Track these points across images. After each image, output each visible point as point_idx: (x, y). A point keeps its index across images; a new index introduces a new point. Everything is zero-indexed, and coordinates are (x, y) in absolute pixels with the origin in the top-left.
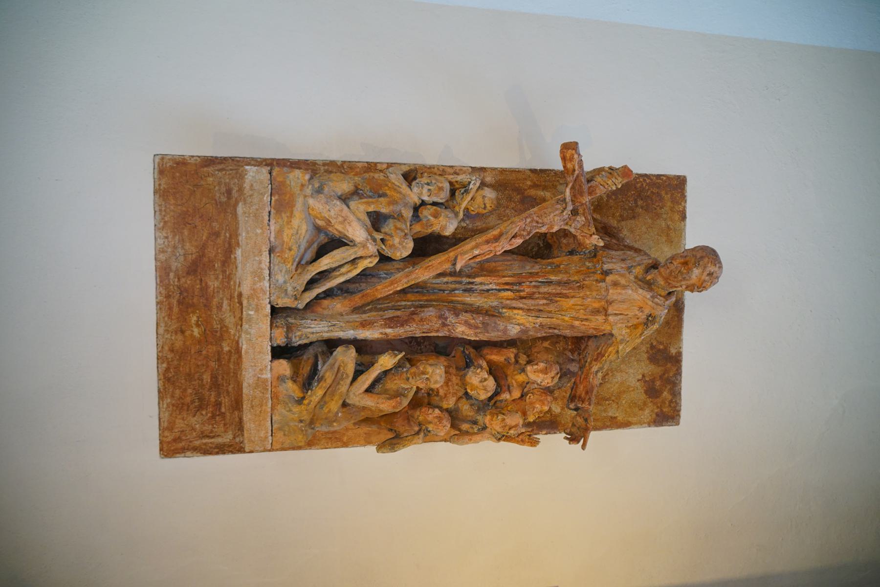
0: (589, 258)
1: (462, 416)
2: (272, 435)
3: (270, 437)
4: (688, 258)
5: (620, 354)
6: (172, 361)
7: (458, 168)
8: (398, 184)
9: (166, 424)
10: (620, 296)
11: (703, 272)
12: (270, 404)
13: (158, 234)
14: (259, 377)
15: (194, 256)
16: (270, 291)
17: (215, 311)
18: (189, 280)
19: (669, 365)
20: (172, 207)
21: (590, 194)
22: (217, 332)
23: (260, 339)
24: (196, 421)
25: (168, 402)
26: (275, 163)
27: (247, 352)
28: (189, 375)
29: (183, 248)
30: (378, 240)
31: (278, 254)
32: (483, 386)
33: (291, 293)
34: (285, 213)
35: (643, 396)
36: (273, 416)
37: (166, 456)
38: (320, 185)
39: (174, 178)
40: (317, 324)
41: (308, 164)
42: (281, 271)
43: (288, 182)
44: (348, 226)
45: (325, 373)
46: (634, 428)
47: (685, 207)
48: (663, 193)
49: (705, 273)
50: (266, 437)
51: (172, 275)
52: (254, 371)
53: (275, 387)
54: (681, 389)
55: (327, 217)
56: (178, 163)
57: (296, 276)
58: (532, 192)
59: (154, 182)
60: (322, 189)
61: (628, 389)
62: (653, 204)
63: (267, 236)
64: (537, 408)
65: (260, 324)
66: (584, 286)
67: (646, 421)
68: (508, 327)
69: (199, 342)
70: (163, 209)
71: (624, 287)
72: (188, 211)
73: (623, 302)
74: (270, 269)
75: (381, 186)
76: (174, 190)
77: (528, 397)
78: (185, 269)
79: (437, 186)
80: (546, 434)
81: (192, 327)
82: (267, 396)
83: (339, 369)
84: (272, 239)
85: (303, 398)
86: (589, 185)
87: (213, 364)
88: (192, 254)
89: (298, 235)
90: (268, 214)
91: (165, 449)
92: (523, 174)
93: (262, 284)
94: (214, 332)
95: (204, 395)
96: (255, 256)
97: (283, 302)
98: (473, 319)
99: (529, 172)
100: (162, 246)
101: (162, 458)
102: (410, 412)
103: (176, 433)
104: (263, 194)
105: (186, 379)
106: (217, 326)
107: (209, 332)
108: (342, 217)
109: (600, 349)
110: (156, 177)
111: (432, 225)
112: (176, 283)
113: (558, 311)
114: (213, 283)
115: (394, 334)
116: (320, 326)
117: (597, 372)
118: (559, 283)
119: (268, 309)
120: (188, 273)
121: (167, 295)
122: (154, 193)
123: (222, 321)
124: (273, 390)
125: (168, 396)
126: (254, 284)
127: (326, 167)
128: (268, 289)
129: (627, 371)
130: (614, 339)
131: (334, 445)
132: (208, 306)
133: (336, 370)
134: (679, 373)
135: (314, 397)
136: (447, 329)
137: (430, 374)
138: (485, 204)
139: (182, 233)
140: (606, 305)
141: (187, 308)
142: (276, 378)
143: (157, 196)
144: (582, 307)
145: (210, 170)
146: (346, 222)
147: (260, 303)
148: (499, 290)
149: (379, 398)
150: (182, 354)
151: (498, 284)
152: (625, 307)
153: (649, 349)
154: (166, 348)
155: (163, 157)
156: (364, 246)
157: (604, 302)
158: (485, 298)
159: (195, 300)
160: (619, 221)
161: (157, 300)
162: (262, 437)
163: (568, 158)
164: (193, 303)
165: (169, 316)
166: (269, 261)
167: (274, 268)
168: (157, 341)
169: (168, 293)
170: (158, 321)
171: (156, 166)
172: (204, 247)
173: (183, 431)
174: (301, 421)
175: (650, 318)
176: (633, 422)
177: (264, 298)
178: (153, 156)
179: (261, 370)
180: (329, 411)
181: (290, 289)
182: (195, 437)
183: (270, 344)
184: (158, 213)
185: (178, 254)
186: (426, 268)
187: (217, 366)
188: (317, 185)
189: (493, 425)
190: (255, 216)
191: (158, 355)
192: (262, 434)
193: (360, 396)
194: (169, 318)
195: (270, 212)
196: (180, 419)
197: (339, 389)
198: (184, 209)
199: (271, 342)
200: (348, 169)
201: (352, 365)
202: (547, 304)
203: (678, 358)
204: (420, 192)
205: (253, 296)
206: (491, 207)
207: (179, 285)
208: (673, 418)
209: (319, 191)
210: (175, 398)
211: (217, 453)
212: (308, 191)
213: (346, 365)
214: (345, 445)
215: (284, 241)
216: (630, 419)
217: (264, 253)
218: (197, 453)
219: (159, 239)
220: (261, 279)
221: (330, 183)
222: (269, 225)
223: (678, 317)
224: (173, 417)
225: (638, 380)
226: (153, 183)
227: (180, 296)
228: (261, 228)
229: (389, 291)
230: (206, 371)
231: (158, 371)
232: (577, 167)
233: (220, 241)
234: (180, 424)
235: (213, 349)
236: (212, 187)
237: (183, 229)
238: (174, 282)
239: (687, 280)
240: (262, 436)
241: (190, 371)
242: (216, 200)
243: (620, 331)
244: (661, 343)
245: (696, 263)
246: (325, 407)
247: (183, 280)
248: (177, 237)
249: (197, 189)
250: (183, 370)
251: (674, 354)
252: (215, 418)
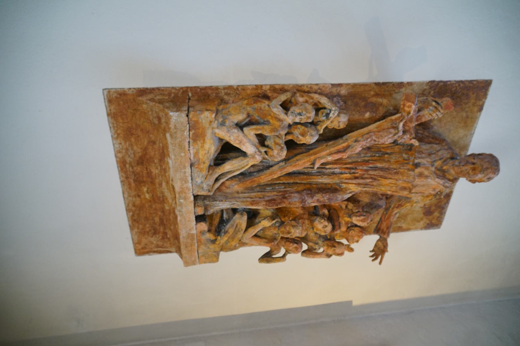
0: (406, 150)
4: (476, 166)
7: (321, 85)
13: (115, 142)
14: (189, 233)
15: (140, 154)
20: (121, 124)
21: (417, 121)
22: (160, 197)
26: (189, 90)
27: (181, 221)
29: (132, 149)
31: (196, 166)
34: (200, 141)
35: (422, 215)
38: (223, 119)
39: (119, 105)
40: (223, 204)
41: (213, 89)
43: (200, 121)
45: (229, 229)
47: (484, 102)
51: (127, 166)
53: (199, 237)
56: (120, 94)
57: (208, 176)
58: (374, 99)
60: (225, 123)
63: (188, 157)
66: (399, 172)
69: (150, 201)
71: (427, 177)
73: (423, 186)
74: (191, 176)
75: (266, 115)
79: (307, 116)
84: (192, 158)
85: (216, 240)
86: (418, 114)
87: (160, 213)
88: (139, 153)
90: (188, 143)
92: (369, 87)
96: (181, 169)
98: (323, 197)
99: (374, 84)
100: (119, 149)
103: (143, 245)
104: (184, 131)
106: (159, 194)
108: (239, 140)
109: (401, 202)
117: (396, 214)
118: (382, 169)
119: (192, 198)
120: (138, 164)
123: (162, 193)
127: (226, 91)
128: (191, 187)
132: (153, 183)
137: (293, 233)
143: (110, 117)
144: (395, 185)
145: (143, 99)
146: (241, 144)
148: (341, 173)
149: (261, 241)
151: (340, 168)
154: (131, 205)
155: (109, 91)
158: (332, 179)
165: (130, 188)
171: (106, 97)
178: (101, 91)
179: (190, 229)
184: (112, 129)
188: (221, 120)
190: (179, 145)
192: (193, 259)
195: (189, 142)
197: (237, 236)
198: (130, 125)
200: (242, 91)
202: (372, 182)
209: (223, 124)
212: (215, 125)
213: (241, 225)
215: (199, 159)
216: (410, 227)
221: (230, 116)
222: (189, 150)
228: (185, 153)
229: (269, 178)
233: (156, 146)
238: (129, 169)
247: (135, 168)
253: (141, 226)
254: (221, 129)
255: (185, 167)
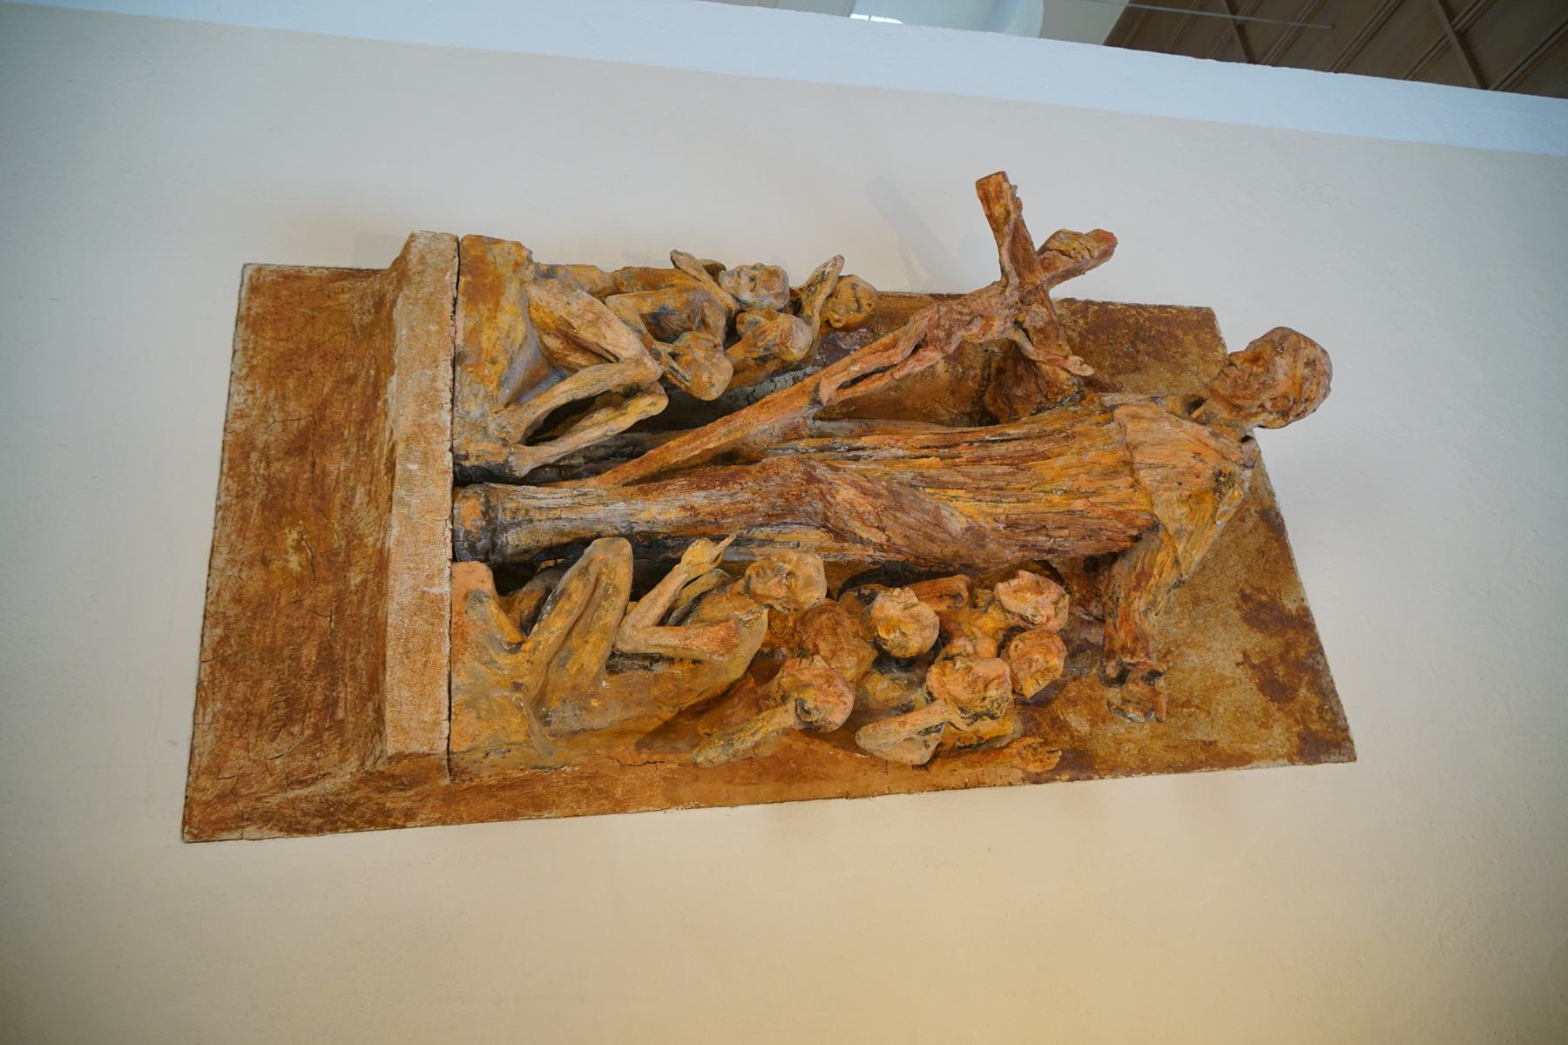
1: (878, 703)
2: (450, 719)
3: (446, 724)
5: (1183, 567)
6: (236, 621)
8: (694, 273)
9: (205, 761)
10: (1151, 435)
11: (1295, 361)
12: (448, 650)
14: (424, 592)
15: (303, 423)
16: (452, 431)
17: (337, 514)
18: (290, 466)
19: (1291, 634)
23: (429, 517)
24: (277, 751)
25: (216, 710)
28: (270, 650)
29: (282, 409)
30: (663, 354)
31: (470, 369)
32: (912, 616)
33: (496, 434)
34: (484, 303)
35: (1260, 699)
36: (454, 675)
37: (197, 838)
40: (549, 493)
42: (476, 396)
43: (490, 258)
44: (604, 329)
46: (1259, 767)
48: (1179, 333)
49: (1300, 364)
50: (436, 724)
51: (254, 456)
52: (415, 579)
53: (459, 614)
54: (1332, 682)
55: (565, 316)
56: (286, 277)
59: (239, 305)
61: (1221, 681)
62: (1166, 349)
64: (1037, 661)
65: (430, 487)
67: (1281, 752)
68: (943, 512)
69: (300, 581)
70: (251, 346)
72: (298, 348)
73: (1160, 444)
74: (453, 390)
76: (276, 317)
77: (1012, 647)
78: (284, 445)
80: (1071, 780)
81: (287, 553)
82: (441, 630)
83: (597, 580)
84: (459, 341)
89: (510, 340)
91: (195, 820)
93: (436, 415)
94: (331, 554)
95: (299, 689)
96: (424, 368)
97: (483, 451)
101: (187, 842)
102: (760, 691)
105: (262, 660)
107: (321, 560)
108: (594, 313)
109: (1139, 565)
110: (243, 295)
111: (764, 332)
112: (262, 472)
113: (1037, 485)
114: (337, 466)
115: (708, 510)
116: (555, 496)
120: (288, 453)
121: (240, 493)
122: (237, 321)
124: (453, 621)
125: (218, 696)
126: (422, 414)
129: (1208, 645)
130: (1161, 534)
131: (594, 808)
133: (593, 579)
134: (1316, 648)
135: (546, 634)
136: (817, 491)
138: (857, 301)
139: (283, 385)
140: (1128, 453)
141: (281, 516)
142: (462, 595)
143: (242, 326)
147: (432, 450)
150: (260, 607)
152: (1166, 452)
153: (1240, 602)
154: (227, 596)
156: (638, 362)
157: (1123, 451)
159: (298, 502)
160: (1112, 375)
161: (219, 503)
162: (426, 722)
163: (993, 194)
164: (293, 508)
165: (241, 532)
166: (451, 377)
167: (461, 390)
168: (208, 582)
169: (243, 490)
170: (216, 544)
171: (246, 281)
172: (325, 403)
173: (243, 775)
174: (517, 687)
175: (1222, 479)
176: (1254, 753)
177: (440, 440)
180: (580, 670)
181: (492, 427)
182: (271, 788)
183: (451, 527)
185: (271, 420)
186: (762, 406)
187: (333, 625)
189: (948, 687)
190: (427, 302)
191: (206, 610)
192: (427, 717)
193: (648, 630)
194: (239, 536)
195: (455, 300)
196: (240, 748)
197: (599, 618)
198: (292, 346)
199: (452, 524)
201: (627, 570)
203: (1306, 620)
204: (735, 285)
205: (419, 433)
206: (870, 305)
207: (266, 474)
208: (1338, 745)
210: (234, 701)
211: (319, 830)
214: (620, 807)
215: (481, 349)
216: (1246, 747)
217: (443, 364)
218: (271, 829)
219: (235, 396)
220: (435, 406)
223: (1277, 540)
224: (224, 743)
225: (1238, 664)
226: (236, 302)
227: (267, 495)
228: (438, 323)
230: (308, 638)
231: (202, 642)
232: (1011, 207)
234: (238, 759)
235: (326, 591)
236: (348, 307)
237: (288, 377)
239: (1271, 387)
240: (426, 718)
241: (273, 642)
242: (353, 326)
243: (1171, 513)
244: (1261, 590)
245: (1275, 349)
246: (571, 662)
247: (276, 466)
248: (273, 392)
249: (319, 313)
250: (259, 641)
251: (1294, 612)
252: (321, 737)
253: (241, 689)
254: (545, 286)
255: (435, 362)
